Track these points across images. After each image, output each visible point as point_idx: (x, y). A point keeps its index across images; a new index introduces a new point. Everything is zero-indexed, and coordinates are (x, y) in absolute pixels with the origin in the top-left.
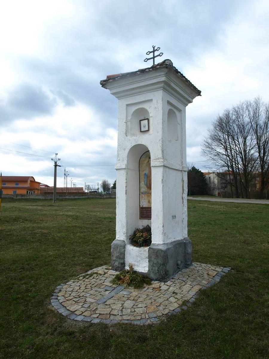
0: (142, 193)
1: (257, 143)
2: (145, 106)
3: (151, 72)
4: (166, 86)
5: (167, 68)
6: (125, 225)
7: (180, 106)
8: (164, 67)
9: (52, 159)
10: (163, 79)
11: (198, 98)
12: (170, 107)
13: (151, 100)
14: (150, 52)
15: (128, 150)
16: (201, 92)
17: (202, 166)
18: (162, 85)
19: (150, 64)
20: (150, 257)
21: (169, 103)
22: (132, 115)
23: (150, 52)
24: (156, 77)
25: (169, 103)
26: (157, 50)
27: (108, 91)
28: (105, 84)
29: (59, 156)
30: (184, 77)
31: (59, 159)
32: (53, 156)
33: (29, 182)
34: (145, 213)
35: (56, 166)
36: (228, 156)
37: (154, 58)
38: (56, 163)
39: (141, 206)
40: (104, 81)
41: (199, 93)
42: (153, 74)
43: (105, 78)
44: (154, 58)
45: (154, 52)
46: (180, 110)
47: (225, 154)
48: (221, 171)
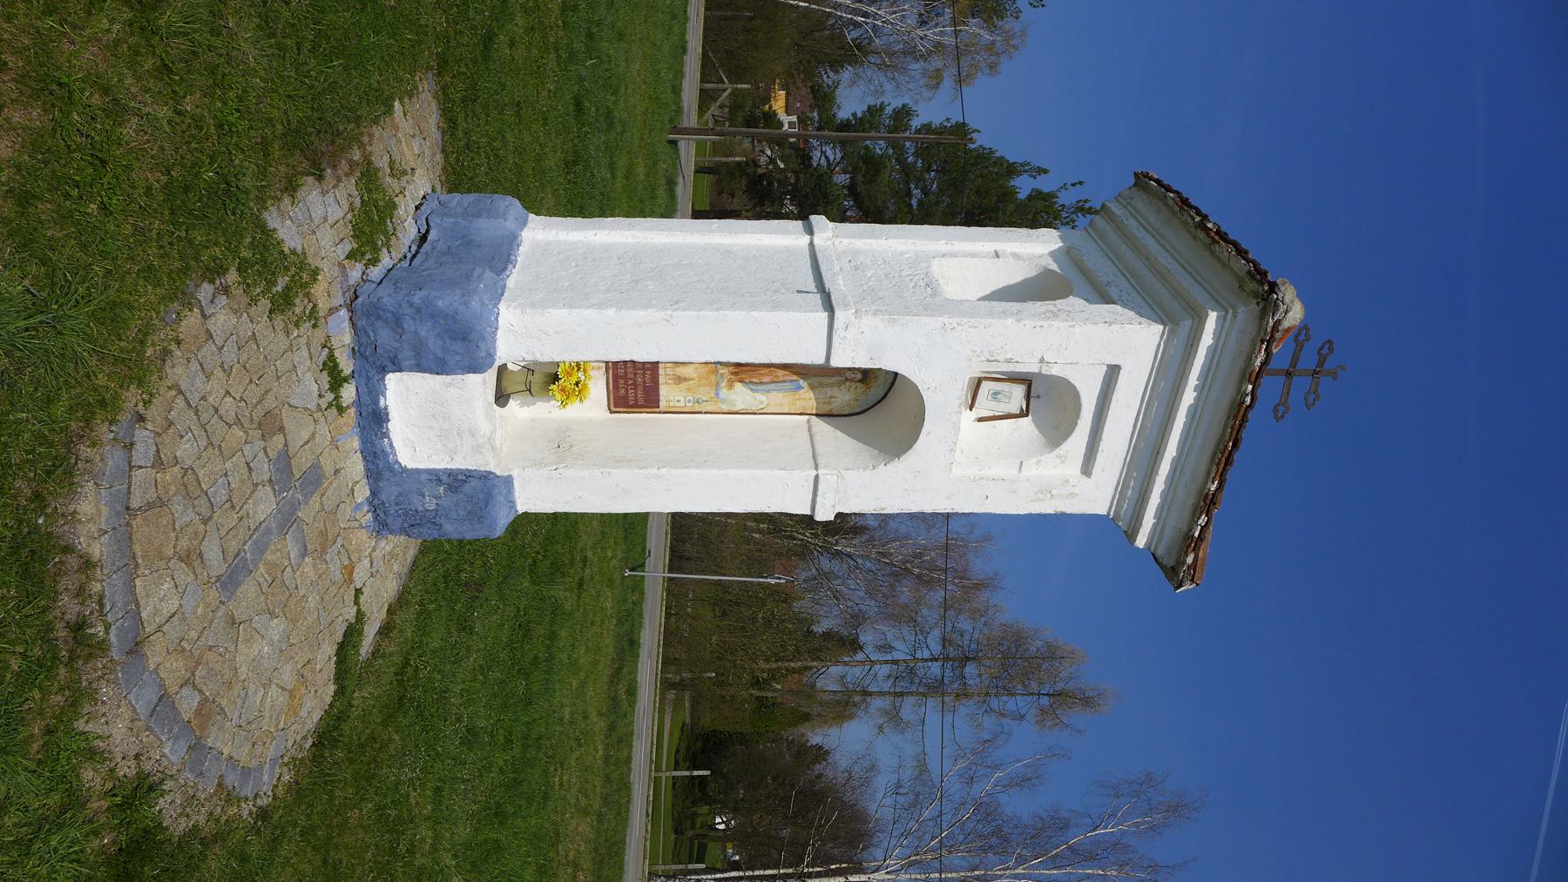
2: (1078, 440)
13: (1087, 470)
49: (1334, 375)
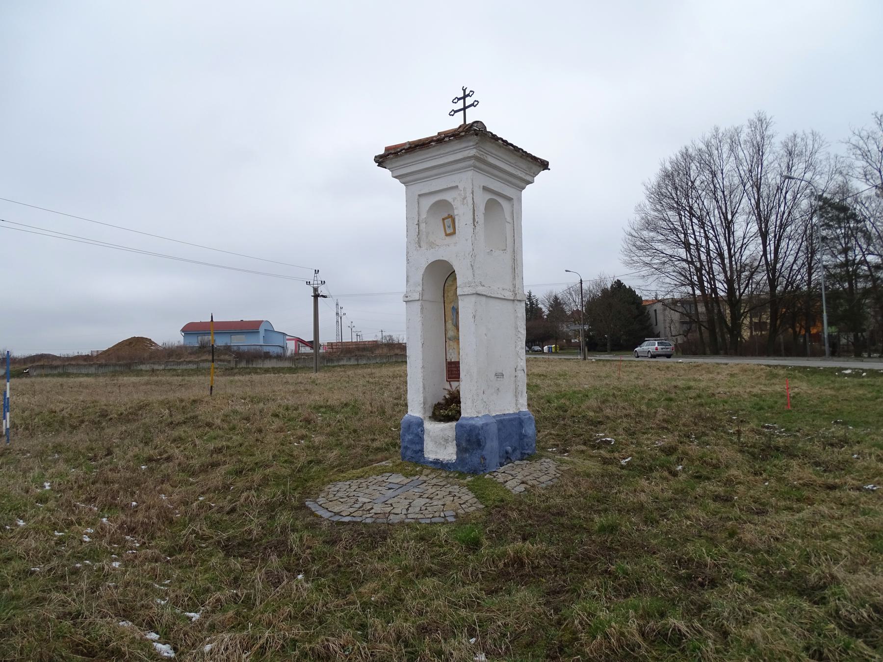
0: (450, 339)
1: (760, 229)
2: (448, 197)
3: (452, 143)
4: (478, 164)
5: (477, 135)
6: (421, 389)
7: (508, 191)
8: (472, 134)
9: (308, 283)
10: (473, 152)
11: (543, 174)
12: (489, 196)
14: (459, 99)
15: (423, 270)
16: (548, 163)
17: (530, 298)
18: (471, 162)
19: (456, 122)
20: (458, 438)
21: (485, 189)
22: (428, 212)
23: (459, 99)
24: (454, 152)
25: (485, 189)
26: (468, 95)
27: (386, 173)
28: (382, 162)
29: (321, 277)
30: (512, 145)
31: (323, 283)
32: (310, 277)
33: (262, 330)
34: (453, 371)
35: (316, 296)
36: (692, 263)
37: (464, 109)
38: (315, 290)
39: (449, 360)
40: (381, 156)
41: (544, 165)
42: (456, 145)
43: (382, 152)
44: (464, 109)
45: (464, 98)
46: (509, 199)
47: (685, 258)
48: (677, 296)
49: (464, 91)
